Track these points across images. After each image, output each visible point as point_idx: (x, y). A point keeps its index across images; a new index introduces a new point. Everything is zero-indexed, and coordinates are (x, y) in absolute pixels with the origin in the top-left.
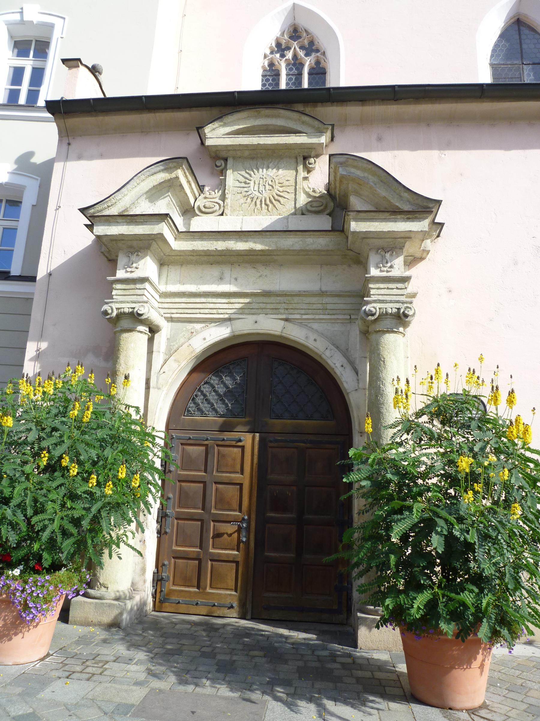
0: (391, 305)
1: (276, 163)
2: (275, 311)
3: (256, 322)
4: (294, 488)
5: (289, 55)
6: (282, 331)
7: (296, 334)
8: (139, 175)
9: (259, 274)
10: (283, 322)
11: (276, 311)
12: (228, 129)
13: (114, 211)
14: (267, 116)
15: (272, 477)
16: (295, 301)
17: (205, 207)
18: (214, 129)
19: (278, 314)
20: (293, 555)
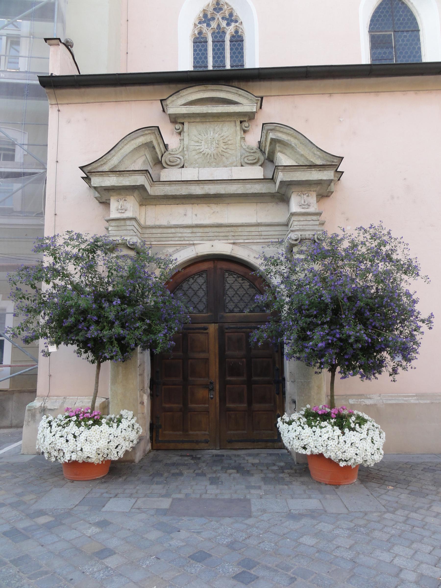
0: (309, 233)
1: (220, 127)
2: (225, 238)
3: (212, 246)
4: (244, 360)
5: (214, 25)
6: (231, 251)
7: (241, 253)
8: (123, 140)
9: (212, 211)
10: (231, 246)
11: (226, 237)
12: (183, 101)
13: (106, 168)
14: (213, 90)
15: (227, 353)
16: (240, 230)
17: (170, 161)
18: (173, 101)
19: (227, 240)
20: (245, 405)
